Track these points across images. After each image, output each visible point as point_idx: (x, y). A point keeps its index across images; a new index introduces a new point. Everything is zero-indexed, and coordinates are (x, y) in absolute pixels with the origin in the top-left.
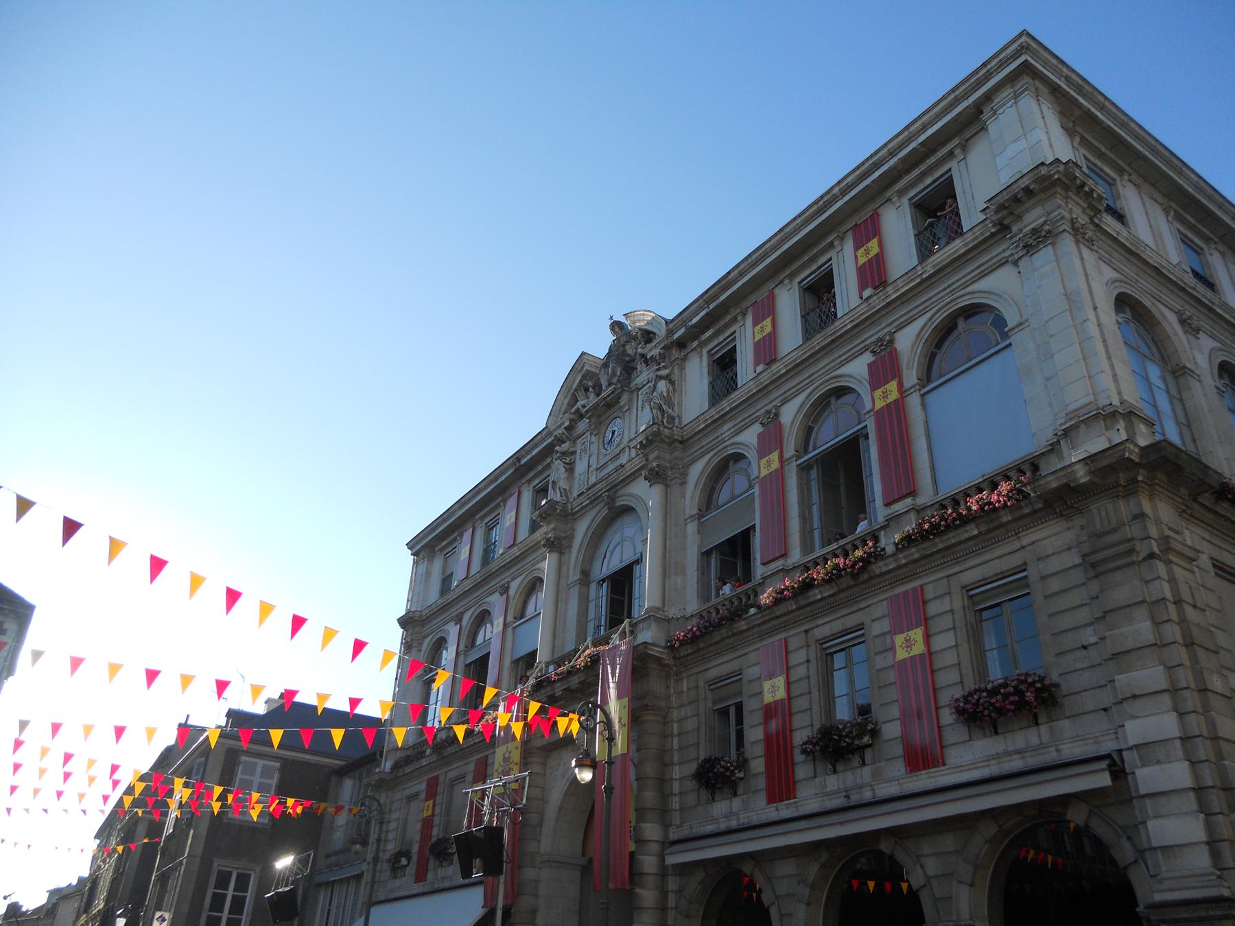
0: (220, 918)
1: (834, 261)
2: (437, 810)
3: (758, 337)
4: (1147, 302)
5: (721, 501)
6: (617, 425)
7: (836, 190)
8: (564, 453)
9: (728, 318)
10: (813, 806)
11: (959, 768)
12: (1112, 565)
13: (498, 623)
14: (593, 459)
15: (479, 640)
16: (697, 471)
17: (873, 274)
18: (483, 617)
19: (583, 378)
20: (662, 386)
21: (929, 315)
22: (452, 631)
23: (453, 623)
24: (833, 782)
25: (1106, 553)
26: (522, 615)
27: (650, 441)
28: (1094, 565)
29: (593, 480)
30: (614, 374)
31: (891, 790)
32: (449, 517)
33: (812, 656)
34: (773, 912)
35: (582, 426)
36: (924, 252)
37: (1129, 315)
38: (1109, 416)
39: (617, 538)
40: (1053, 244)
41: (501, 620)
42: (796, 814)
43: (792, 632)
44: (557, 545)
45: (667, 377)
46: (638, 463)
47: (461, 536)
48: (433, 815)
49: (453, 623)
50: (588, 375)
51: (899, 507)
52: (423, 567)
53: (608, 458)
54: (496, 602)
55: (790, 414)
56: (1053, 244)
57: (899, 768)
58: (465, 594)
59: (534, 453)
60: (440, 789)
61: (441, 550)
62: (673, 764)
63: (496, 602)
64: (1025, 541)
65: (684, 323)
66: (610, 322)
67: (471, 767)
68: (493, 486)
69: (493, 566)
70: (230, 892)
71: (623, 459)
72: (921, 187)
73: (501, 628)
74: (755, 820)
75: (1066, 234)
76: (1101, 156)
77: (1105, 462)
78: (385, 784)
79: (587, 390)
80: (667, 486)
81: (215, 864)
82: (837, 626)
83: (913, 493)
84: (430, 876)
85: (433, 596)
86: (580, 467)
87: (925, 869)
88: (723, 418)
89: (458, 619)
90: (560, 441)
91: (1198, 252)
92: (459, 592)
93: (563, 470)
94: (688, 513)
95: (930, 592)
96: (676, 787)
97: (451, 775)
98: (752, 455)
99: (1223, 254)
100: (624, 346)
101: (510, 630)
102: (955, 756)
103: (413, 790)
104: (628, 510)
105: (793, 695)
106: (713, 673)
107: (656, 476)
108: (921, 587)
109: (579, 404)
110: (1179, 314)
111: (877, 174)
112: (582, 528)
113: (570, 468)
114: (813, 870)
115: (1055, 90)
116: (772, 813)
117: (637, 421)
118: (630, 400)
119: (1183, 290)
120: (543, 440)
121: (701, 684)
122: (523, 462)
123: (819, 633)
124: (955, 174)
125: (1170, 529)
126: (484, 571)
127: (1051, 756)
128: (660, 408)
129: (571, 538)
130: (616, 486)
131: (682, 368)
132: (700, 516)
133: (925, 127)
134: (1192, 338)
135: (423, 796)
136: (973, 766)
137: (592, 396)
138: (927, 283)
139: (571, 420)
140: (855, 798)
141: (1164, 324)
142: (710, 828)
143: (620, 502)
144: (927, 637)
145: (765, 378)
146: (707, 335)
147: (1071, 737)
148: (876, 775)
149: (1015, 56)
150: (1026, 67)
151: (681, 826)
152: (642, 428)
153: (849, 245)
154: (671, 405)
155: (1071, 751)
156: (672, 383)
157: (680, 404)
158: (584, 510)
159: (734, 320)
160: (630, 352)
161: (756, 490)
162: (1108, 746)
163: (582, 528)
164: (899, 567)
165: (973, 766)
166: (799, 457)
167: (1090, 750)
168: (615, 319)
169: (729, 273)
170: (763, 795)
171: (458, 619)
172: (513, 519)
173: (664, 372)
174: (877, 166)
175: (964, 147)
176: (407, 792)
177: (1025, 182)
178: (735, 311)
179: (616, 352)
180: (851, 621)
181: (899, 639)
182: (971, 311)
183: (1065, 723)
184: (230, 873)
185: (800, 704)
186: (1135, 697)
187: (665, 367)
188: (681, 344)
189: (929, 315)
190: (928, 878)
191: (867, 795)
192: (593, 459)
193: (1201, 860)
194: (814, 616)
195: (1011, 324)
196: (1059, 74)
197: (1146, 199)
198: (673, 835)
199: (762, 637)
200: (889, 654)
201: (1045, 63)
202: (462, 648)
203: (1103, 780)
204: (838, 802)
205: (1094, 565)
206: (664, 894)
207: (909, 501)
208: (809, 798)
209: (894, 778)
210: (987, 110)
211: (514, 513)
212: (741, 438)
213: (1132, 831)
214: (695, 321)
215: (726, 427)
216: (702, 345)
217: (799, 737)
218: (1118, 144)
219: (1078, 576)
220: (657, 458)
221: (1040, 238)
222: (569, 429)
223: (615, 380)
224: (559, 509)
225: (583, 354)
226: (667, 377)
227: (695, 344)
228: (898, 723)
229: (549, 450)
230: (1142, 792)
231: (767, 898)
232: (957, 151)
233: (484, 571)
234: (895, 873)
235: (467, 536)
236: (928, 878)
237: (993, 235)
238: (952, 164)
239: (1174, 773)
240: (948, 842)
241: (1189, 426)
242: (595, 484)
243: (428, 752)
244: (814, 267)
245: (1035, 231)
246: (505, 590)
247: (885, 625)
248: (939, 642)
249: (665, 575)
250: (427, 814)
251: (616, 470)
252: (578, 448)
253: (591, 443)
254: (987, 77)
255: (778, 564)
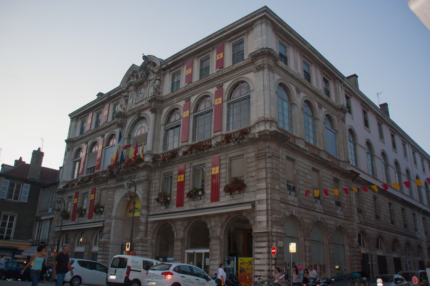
0: (5, 229)
1: (210, 56)
2: (79, 201)
3: (187, 74)
4: (287, 85)
5: (172, 121)
6: (143, 90)
7: (213, 36)
8: (125, 96)
9: (179, 65)
10: (187, 208)
11: (222, 202)
12: (261, 158)
13: (100, 147)
14: (134, 100)
15: (94, 150)
16: (165, 111)
17: (220, 64)
18: (95, 144)
19: (133, 71)
20: (157, 82)
21: (232, 80)
22: (84, 147)
23: (84, 144)
24: (193, 203)
25: (260, 155)
26: (108, 145)
27: (154, 99)
28: (257, 157)
29: (134, 107)
30: (143, 74)
31: (206, 206)
32: (84, 109)
33: (192, 170)
34: (175, 233)
35: (132, 88)
36: (234, 63)
37: (282, 88)
38: (266, 121)
39: (140, 126)
40: (263, 70)
41: (101, 146)
42: (183, 210)
43: (187, 163)
44: (121, 126)
45: (159, 80)
46: (148, 105)
47: (88, 115)
48: (77, 203)
49: (84, 144)
50: (134, 72)
51: (218, 134)
52: (74, 123)
53: (139, 101)
54: (100, 140)
55: (226, 86)
56: (263, 70)
57: (209, 201)
58: (89, 135)
59: (115, 93)
60: (79, 195)
61: (81, 119)
62: (152, 195)
63: (100, 140)
64: (244, 149)
65: (166, 63)
66: (143, 56)
67: (91, 190)
68: (100, 101)
69: (99, 128)
70: (8, 222)
71: (143, 103)
72: (236, 41)
73: (101, 148)
74: (173, 211)
75: (266, 69)
76: (283, 40)
77: (262, 134)
78: (61, 192)
79: (133, 76)
80: (156, 114)
81: (3, 213)
82: (198, 163)
83: (221, 131)
84: (76, 220)
85: (78, 134)
86: (130, 101)
87: (211, 224)
88: (174, 97)
89: (87, 143)
90: (124, 92)
91: (308, 66)
92: (87, 134)
93: (124, 101)
94: (162, 123)
95: (222, 158)
96: (152, 201)
97: (84, 192)
98: (181, 110)
99: (315, 66)
100: (146, 65)
101: (104, 149)
102: (221, 199)
103: (71, 195)
104: (144, 118)
105: (186, 180)
106: (165, 171)
107: (153, 111)
108: (220, 156)
109: (131, 80)
110: (296, 87)
111: (224, 34)
112: (129, 121)
113: (127, 101)
114: (186, 223)
115: (272, 22)
116: (177, 209)
117: (148, 91)
118: (147, 84)
119: (299, 80)
120: (118, 90)
121: (162, 174)
122: (111, 95)
123: (194, 164)
124: (245, 39)
125: (275, 150)
126: (96, 129)
127: (241, 201)
128: (156, 89)
129: (126, 124)
130: (141, 110)
131: (164, 77)
132: (165, 124)
133: (238, 25)
134: (298, 94)
135: (74, 197)
136: (225, 202)
137: (135, 79)
138: (233, 71)
139: (128, 86)
140: (198, 207)
141: (291, 91)
142: (161, 212)
143: (142, 115)
144: (220, 169)
145: (188, 88)
146: (173, 68)
147: (247, 197)
148: (203, 202)
149: (263, 12)
150: (266, 16)
151: (153, 211)
152: (150, 95)
153: (215, 52)
154: (159, 88)
155: (246, 200)
156: (160, 81)
157: (162, 88)
158: (130, 116)
159: (181, 66)
160: (148, 67)
161: (182, 120)
162: (253, 199)
163: (129, 121)
164: (215, 150)
165: (225, 202)
166: (194, 113)
167: (249, 200)
168: (145, 55)
169: (180, 52)
170: (175, 205)
171: (87, 143)
172: (107, 113)
173: (158, 78)
174: (225, 32)
175: (248, 33)
176: (68, 195)
177: (259, 52)
178: (181, 63)
179: (144, 66)
180: (202, 162)
181: (213, 169)
182: (243, 82)
183: (246, 193)
184: (7, 216)
185: (187, 183)
186: (260, 189)
187: (159, 76)
188: (164, 69)
189: (232, 80)
190: (212, 226)
191: (201, 207)
192: (134, 100)
193: (265, 224)
194: (193, 160)
195: (251, 90)
196: (274, 18)
197: (295, 51)
198: (151, 213)
199: (179, 163)
200: (210, 172)
201: (270, 15)
202: (88, 152)
203: (250, 207)
204: (194, 208)
205: (257, 157)
206: (147, 228)
207: (220, 132)
208: (186, 207)
209: (208, 203)
210: (255, 24)
211: (107, 111)
212: (178, 104)
213: (254, 218)
214: (169, 63)
215: (175, 99)
216: (170, 71)
217: (186, 191)
218: (288, 37)
219: (254, 159)
220: (154, 105)
221: (260, 68)
222: (127, 88)
223: (143, 76)
224: (122, 114)
225: (133, 65)
226: (159, 80)
227: (169, 70)
228: (210, 190)
229: (120, 93)
230: (257, 210)
231: (174, 229)
232: (246, 34)
233: (96, 129)
234: (206, 224)
235: (91, 115)
236: (212, 226)
237: (250, 62)
238: (244, 37)
239: (264, 207)
240: (217, 219)
241: (291, 119)
242: (134, 109)
243: (76, 184)
244: (205, 56)
245: (260, 66)
246: (103, 136)
247: (210, 165)
248: (223, 171)
249: (153, 141)
250: (75, 202)
251: (141, 105)
252: (130, 95)
253: (134, 94)
254: (255, 16)
255: (185, 143)
